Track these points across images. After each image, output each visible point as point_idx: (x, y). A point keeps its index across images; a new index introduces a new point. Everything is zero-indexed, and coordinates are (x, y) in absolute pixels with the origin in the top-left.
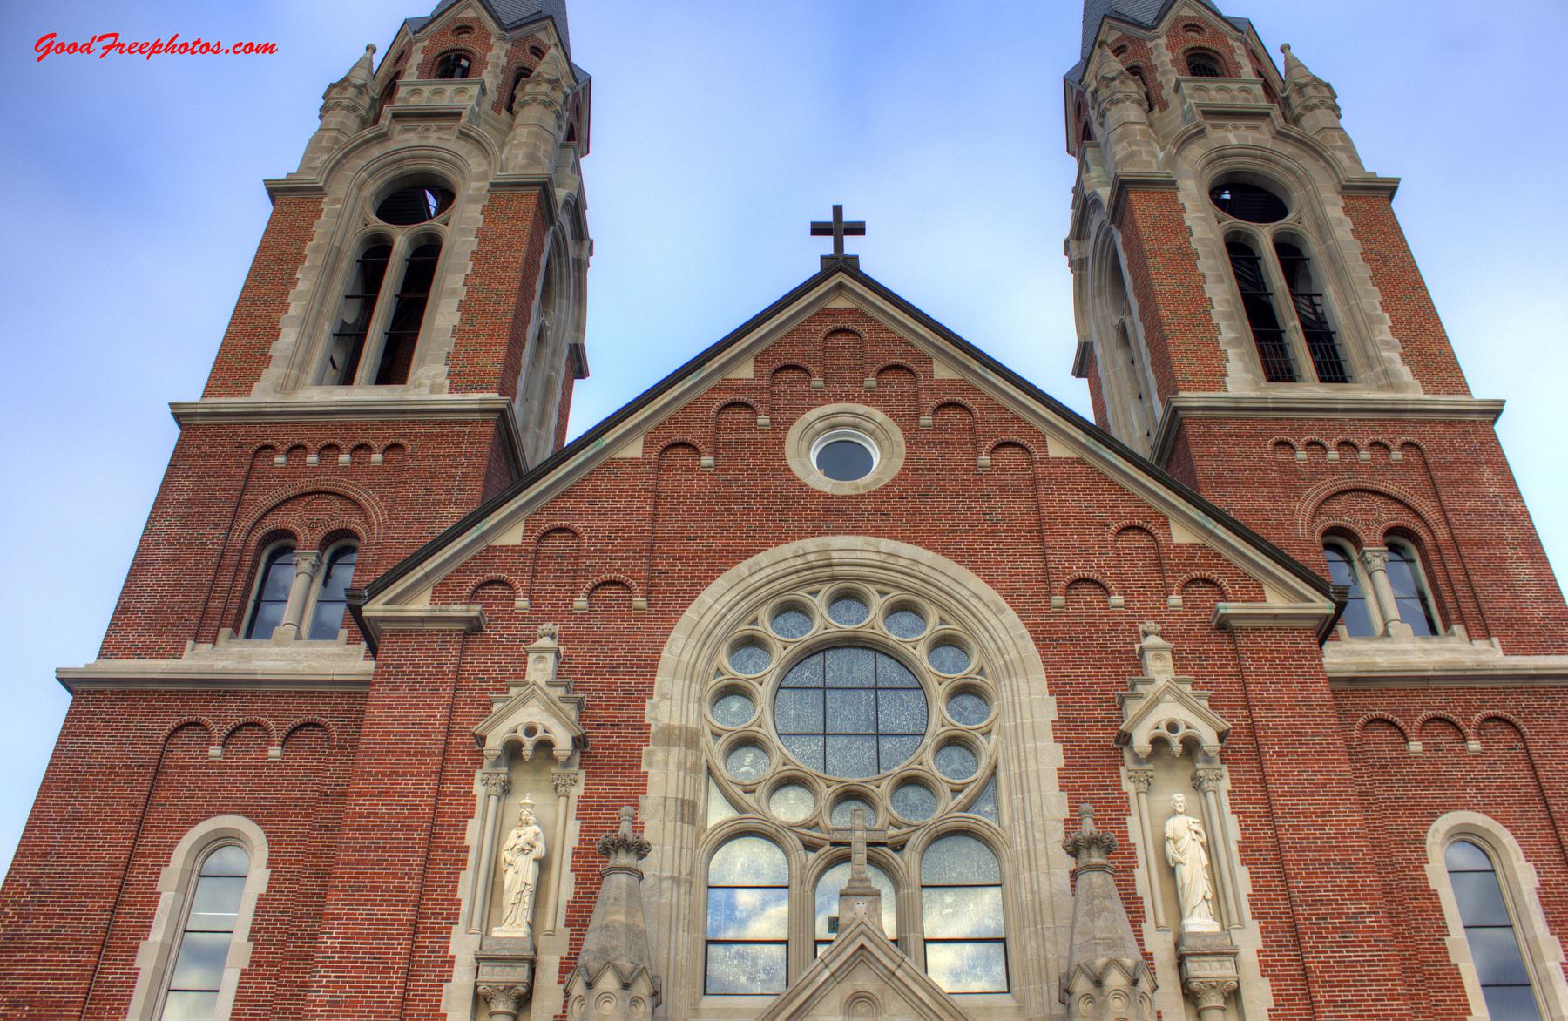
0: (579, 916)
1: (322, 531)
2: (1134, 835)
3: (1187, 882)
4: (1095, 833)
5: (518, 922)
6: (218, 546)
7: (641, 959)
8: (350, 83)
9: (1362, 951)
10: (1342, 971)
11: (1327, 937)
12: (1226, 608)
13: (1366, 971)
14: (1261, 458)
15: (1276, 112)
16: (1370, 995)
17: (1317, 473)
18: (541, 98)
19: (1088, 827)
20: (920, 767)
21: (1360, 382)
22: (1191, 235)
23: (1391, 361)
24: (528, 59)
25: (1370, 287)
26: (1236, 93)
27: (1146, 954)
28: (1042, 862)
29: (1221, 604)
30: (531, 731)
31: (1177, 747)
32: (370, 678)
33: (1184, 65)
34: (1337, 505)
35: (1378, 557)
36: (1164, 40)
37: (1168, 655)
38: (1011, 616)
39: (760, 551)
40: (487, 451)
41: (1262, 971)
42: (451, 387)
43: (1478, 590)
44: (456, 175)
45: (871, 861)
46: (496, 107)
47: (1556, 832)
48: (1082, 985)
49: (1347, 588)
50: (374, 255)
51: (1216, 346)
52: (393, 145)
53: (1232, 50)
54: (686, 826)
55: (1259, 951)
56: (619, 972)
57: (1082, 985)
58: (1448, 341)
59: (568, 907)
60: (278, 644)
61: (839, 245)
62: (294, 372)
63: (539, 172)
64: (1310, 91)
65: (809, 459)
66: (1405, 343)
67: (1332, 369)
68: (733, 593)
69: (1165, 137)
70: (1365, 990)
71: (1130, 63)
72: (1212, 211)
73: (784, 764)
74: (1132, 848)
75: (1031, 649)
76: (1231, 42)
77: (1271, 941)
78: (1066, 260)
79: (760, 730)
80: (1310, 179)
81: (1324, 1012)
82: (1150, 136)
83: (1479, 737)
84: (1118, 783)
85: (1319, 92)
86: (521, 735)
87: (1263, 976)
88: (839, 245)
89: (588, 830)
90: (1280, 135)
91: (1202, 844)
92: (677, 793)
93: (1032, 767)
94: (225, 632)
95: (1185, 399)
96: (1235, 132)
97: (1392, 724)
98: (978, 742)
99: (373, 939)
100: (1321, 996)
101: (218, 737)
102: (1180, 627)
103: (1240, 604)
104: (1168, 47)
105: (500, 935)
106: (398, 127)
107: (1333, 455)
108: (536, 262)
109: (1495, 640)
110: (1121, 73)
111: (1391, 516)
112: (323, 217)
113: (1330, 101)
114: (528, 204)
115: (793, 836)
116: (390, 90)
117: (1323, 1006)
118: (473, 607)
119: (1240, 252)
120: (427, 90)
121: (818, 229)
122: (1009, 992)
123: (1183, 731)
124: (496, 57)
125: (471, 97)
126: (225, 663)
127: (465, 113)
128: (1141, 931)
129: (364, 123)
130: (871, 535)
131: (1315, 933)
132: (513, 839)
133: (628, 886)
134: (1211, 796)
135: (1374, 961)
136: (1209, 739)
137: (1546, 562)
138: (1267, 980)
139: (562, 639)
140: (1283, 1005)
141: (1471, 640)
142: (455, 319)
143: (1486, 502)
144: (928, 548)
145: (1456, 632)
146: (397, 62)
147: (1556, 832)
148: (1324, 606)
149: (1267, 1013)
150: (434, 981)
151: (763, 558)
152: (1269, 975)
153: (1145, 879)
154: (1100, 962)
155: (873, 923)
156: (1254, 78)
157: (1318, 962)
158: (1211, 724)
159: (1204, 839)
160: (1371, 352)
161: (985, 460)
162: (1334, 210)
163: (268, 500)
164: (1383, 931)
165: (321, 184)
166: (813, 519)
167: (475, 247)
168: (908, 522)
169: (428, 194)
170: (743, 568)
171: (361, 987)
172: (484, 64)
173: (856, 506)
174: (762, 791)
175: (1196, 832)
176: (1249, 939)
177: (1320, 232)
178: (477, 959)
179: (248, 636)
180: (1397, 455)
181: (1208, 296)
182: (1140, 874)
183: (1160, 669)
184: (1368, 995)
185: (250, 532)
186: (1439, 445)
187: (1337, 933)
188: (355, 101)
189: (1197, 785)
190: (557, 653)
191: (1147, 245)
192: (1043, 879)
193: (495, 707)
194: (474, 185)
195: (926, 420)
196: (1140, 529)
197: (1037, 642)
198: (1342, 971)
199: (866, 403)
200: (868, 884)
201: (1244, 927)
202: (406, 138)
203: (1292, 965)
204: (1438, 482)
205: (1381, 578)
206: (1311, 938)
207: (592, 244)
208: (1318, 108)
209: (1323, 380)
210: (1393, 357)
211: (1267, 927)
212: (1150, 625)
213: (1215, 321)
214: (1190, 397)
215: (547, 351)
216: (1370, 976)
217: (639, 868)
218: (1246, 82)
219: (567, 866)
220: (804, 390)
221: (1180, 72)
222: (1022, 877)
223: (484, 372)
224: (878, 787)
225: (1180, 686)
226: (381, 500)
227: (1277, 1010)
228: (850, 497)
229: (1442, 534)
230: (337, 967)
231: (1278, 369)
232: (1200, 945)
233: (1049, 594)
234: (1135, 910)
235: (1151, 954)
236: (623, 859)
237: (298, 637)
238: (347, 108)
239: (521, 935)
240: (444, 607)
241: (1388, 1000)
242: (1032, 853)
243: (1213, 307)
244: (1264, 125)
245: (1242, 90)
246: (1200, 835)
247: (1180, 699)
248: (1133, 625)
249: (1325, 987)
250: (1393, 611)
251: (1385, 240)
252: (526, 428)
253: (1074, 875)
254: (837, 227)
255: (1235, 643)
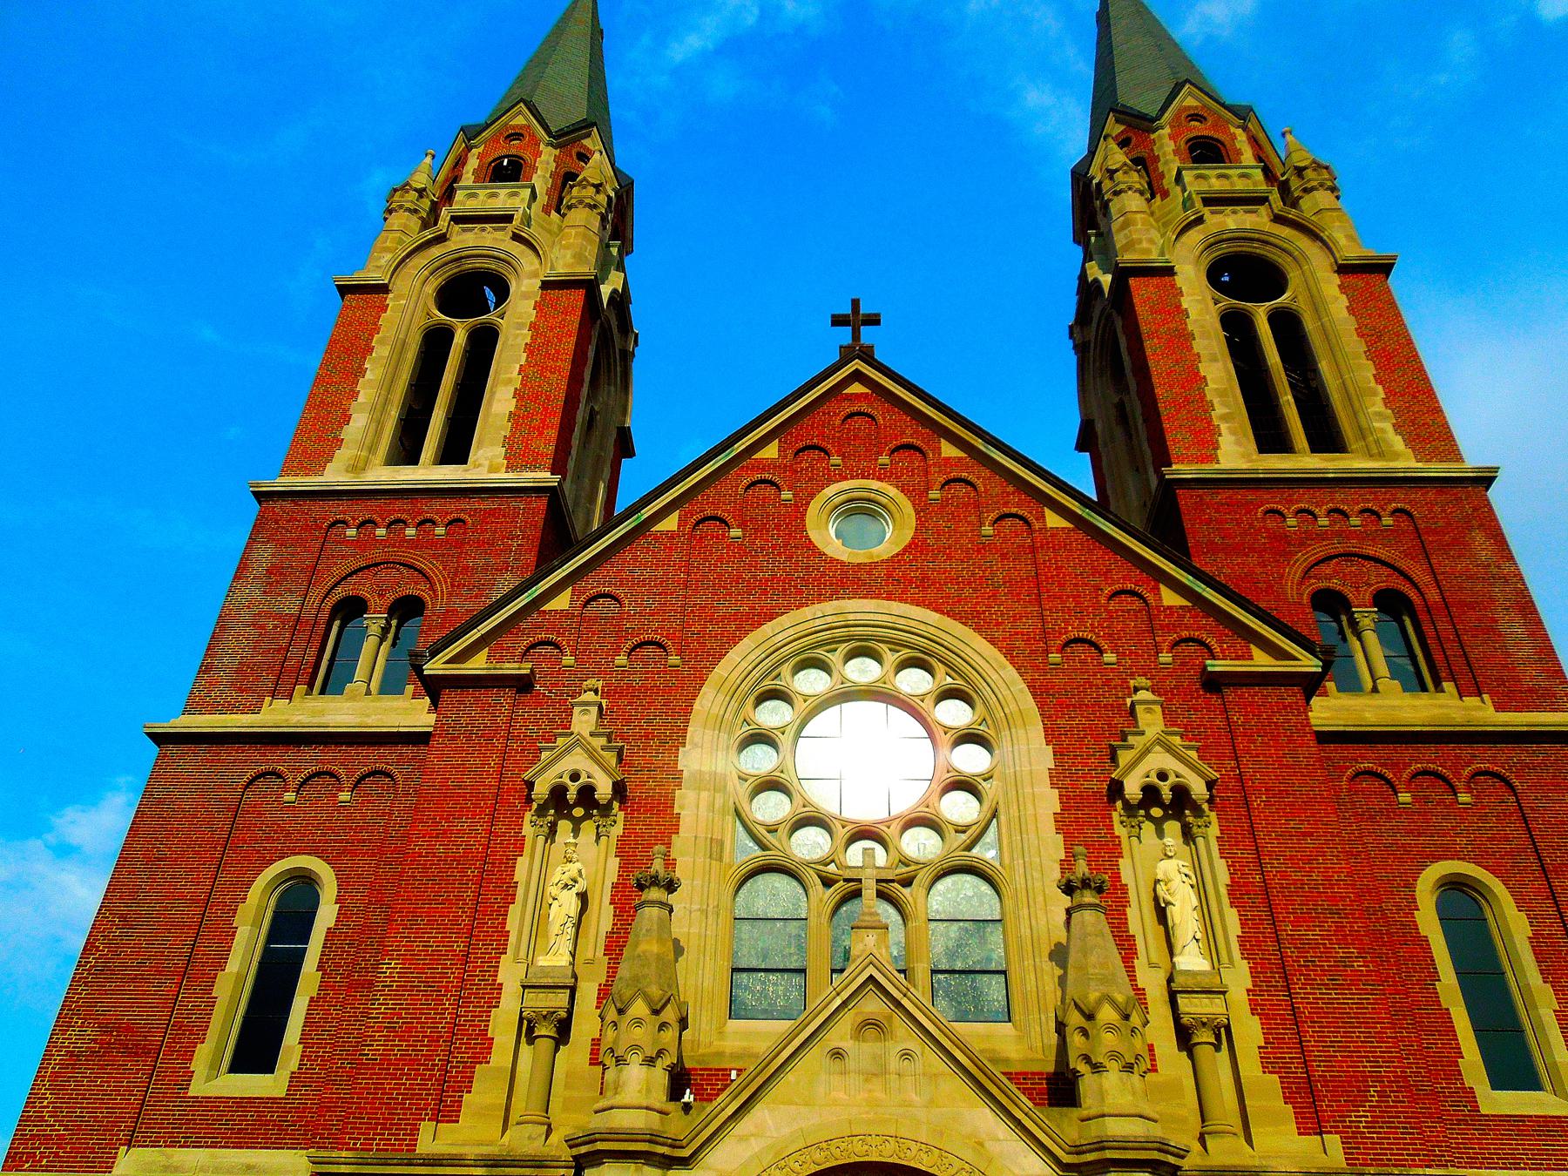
0: (615, 945)
1: (391, 597)
2: (1126, 877)
3: (1177, 922)
4: (1087, 875)
5: (560, 952)
6: (295, 611)
7: (670, 986)
8: (411, 187)
9: (1351, 994)
10: (1331, 1013)
11: (1316, 980)
12: (1214, 666)
13: (1355, 1013)
14: (1251, 525)
15: (1275, 196)
16: (1359, 1037)
17: (1305, 538)
18: (587, 201)
19: (1082, 868)
20: (927, 810)
21: (1352, 452)
22: (1188, 317)
23: (1383, 431)
24: (572, 164)
25: (1363, 361)
26: (1235, 178)
27: (1139, 989)
28: (1040, 899)
29: (1208, 662)
30: (575, 776)
31: (1167, 795)
32: (431, 729)
33: (1186, 154)
34: (1327, 569)
35: (1367, 617)
36: (1167, 130)
37: (1158, 709)
38: (1010, 672)
39: (783, 613)
40: (541, 525)
41: (1252, 1009)
42: (507, 467)
43: (1467, 649)
44: (509, 273)
45: (881, 895)
46: (546, 210)
47: (1549, 883)
48: (1075, 1019)
49: (1334, 647)
50: (435, 343)
51: (1210, 422)
52: (451, 246)
53: (1234, 137)
54: (714, 862)
55: (1248, 991)
56: (648, 1000)
57: (1075, 1019)
58: (1442, 411)
59: (607, 937)
60: (353, 698)
61: (856, 336)
62: (364, 453)
63: (586, 269)
64: (1309, 174)
65: (828, 530)
66: (1398, 413)
67: (1326, 437)
68: (758, 652)
69: (1165, 225)
70: (1354, 1032)
71: (1134, 155)
72: (1208, 292)
73: (804, 806)
74: (1124, 888)
75: (1028, 702)
76: (1233, 129)
77: (1261, 981)
78: (1070, 344)
79: (782, 775)
80: (1306, 258)
81: (1313, 1051)
82: (1151, 225)
83: (1469, 790)
84: (1111, 827)
85: (1319, 175)
86: (566, 780)
87: (1253, 1014)
88: (856, 336)
89: (624, 867)
90: (1278, 219)
91: (1192, 886)
92: (706, 833)
93: (1030, 811)
94: (301, 689)
95: (1178, 472)
96: (1235, 216)
97: (1381, 777)
98: (980, 787)
99: (428, 969)
100: (1310, 1036)
101: (293, 785)
102: (1170, 683)
103: (1228, 662)
104: (1171, 137)
105: (546, 964)
106: (457, 228)
107: (1323, 521)
108: (585, 354)
109: (1486, 697)
110: (1125, 164)
111: (1379, 579)
112: (388, 312)
113: (1329, 183)
114: (577, 298)
115: (811, 872)
116: (448, 195)
117: (1313, 1046)
118: (523, 665)
119: (1237, 329)
120: (482, 193)
121: (838, 321)
122: (1010, 1021)
123: (1172, 779)
124: (546, 161)
125: (523, 200)
126: (300, 717)
127: (517, 217)
128: (1134, 967)
129: (425, 225)
130: (883, 599)
131: (1304, 975)
132: (559, 874)
133: (659, 918)
134: (1200, 841)
135: (1363, 1003)
136: (1198, 788)
137: (1539, 622)
138: (1257, 1017)
139: (606, 695)
140: (1273, 1043)
141: (1461, 698)
142: (511, 405)
143: (1478, 565)
144: (936, 610)
145: (1446, 690)
146: (455, 167)
147: (1549, 883)
148: (1309, 663)
149: (1257, 1051)
150: (483, 1007)
151: (784, 621)
152: (1258, 1014)
153: (1139, 919)
154: (1093, 996)
155: (881, 955)
156: (1253, 163)
157: (1307, 1003)
158: (1200, 774)
159: (1194, 882)
160: (1364, 424)
161: (987, 530)
162: (1330, 285)
163: (337, 572)
164: (1371, 976)
165: (386, 282)
166: (831, 585)
167: (528, 340)
168: (917, 587)
169: (487, 290)
170: (768, 628)
171: (416, 1014)
172: (535, 169)
173: (870, 573)
174: (783, 831)
175: (1186, 875)
176: (1239, 978)
177: (1316, 310)
178: (524, 987)
179: (322, 692)
180: (1387, 521)
181: (1203, 374)
182: (1132, 912)
183: (1151, 722)
184: (1357, 1037)
185: (325, 598)
186: (1430, 511)
187: (1326, 975)
188: (416, 205)
189: (1188, 835)
190: (600, 707)
191: (1144, 329)
192: (1041, 914)
193: (544, 755)
194: (526, 282)
195: (934, 494)
196: (1132, 593)
197: (1034, 695)
198: (1331, 1013)
199: (879, 479)
200: (877, 918)
201: (1234, 967)
202: (464, 239)
203: (1281, 1005)
204: (1428, 548)
205: (1371, 638)
206: (1300, 980)
207: (637, 335)
208: (1317, 189)
209: (1314, 450)
210: (1386, 429)
211: (1256, 968)
212: (1142, 681)
213: (1209, 398)
214: (1182, 470)
215: (597, 433)
216: (1358, 1018)
217: (670, 902)
218: (1246, 167)
219: (607, 899)
220: (824, 468)
221: (1183, 160)
222: (1021, 913)
223: (537, 453)
224: (889, 827)
225: (1169, 738)
226: (444, 569)
227: (1267, 1048)
228: (865, 564)
229: (1433, 595)
230: (395, 995)
231: (1270, 437)
232: (1191, 983)
233: (1047, 652)
234: (1127, 948)
235: (1144, 989)
236: (655, 894)
237: (368, 693)
238: (409, 210)
239: (564, 964)
240: (498, 666)
241: (1377, 1042)
242: (1030, 891)
243: (1207, 385)
244: (1263, 209)
245: (1245, 176)
246: (1190, 878)
247: (1169, 749)
248: (1125, 681)
249: (1314, 1027)
250: (1382, 669)
251: (1380, 316)
252: (576, 504)
253: (1069, 912)
254: (855, 319)
255: (1223, 698)
